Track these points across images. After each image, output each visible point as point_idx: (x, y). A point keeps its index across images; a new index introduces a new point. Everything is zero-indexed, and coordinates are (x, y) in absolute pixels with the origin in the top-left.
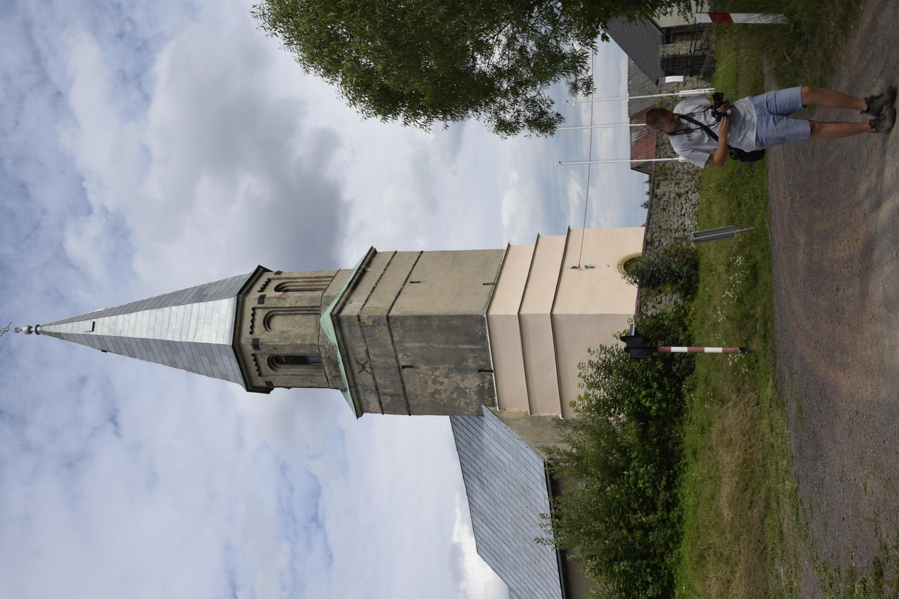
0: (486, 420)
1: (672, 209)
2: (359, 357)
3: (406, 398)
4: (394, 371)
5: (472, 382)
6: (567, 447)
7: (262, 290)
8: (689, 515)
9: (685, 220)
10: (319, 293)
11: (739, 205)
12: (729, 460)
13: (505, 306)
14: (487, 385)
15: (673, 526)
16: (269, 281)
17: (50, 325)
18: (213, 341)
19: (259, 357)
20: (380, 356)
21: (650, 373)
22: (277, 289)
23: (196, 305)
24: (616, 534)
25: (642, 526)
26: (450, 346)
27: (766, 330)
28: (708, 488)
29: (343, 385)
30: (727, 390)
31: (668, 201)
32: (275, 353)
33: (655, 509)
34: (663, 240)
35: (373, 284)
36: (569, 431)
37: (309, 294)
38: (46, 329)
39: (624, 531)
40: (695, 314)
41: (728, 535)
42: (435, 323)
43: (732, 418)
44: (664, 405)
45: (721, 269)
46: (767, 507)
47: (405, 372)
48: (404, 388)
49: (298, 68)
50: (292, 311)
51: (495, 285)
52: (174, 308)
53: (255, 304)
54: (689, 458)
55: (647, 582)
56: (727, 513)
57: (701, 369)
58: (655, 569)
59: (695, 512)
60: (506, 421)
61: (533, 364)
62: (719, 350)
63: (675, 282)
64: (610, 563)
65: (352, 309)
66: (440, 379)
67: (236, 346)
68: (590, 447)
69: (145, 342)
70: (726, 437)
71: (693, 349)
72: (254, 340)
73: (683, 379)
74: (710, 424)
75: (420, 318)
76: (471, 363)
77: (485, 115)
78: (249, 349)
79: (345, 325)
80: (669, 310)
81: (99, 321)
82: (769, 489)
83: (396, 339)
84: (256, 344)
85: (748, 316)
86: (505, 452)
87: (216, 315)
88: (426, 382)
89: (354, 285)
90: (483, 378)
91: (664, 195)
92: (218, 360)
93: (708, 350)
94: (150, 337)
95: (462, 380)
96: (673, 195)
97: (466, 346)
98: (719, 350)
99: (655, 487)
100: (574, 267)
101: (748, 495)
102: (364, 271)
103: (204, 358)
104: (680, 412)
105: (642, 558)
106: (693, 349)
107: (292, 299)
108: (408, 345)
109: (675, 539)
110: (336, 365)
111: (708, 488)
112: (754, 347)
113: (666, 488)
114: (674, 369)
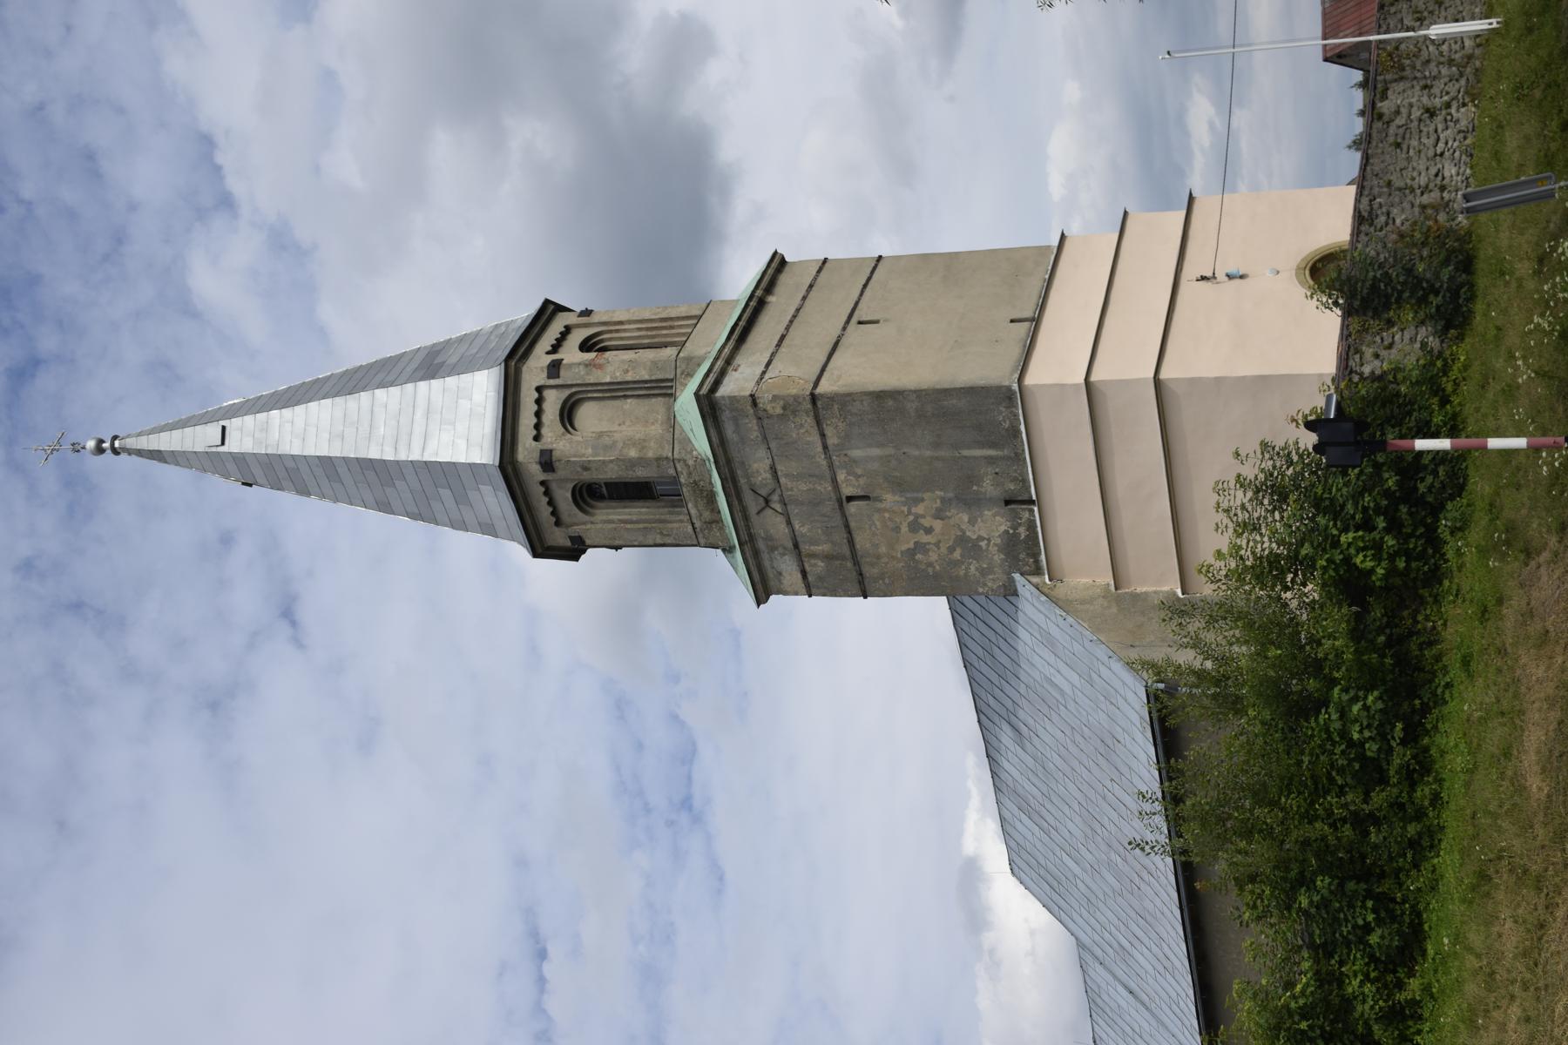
1: (1414, 143)
3: (856, 563)
4: (829, 506)
5: (993, 526)
7: (555, 348)
8: (1454, 789)
9: (1443, 166)
10: (670, 352)
13: (1057, 364)
14: (1023, 532)
15: (1420, 815)
19: (554, 486)
21: (1371, 501)
22: (586, 346)
23: (422, 385)
28: (1495, 735)
29: (728, 539)
31: (1406, 127)
32: (587, 477)
33: (1383, 781)
34: (1395, 211)
35: (781, 329)
36: (1195, 625)
37: (649, 354)
38: (131, 443)
40: (1466, 367)
41: (1540, 831)
42: (911, 406)
45: (1524, 268)
47: (852, 508)
50: (617, 391)
51: (1036, 321)
52: (380, 393)
53: (541, 378)
54: (1455, 672)
56: (1537, 785)
57: (1479, 486)
58: (1384, 903)
59: (1467, 785)
60: (1065, 605)
62: (1520, 443)
65: (738, 383)
66: (926, 522)
69: (327, 464)
70: (1535, 628)
71: (1462, 442)
72: (542, 452)
73: (1442, 507)
74: (1500, 602)
75: (879, 396)
76: (988, 487)
78: (534, 472)
79: (726, 416)
80: (1410, 362)
81: (233, 424)
83: (832, 440)
84: (547, 462)
87: (464, 404)
88: (897, 529)
89: (742, 332)
91: (1398, 112)
93: (1494, 443)
94: (336, 451)
95: (972, 522)
96: (1416, 113)
98: (1520, 443)
100: (1203, 278)
103: (445, 493)
104: (1435, 576)
106: (1462, 442)
107: (615, 366)
108: (856, 453)
109: (1423, 846)
110: (711, 498)
111: (1495, 735)
113: (1403, 742)
114: (1422, 488)
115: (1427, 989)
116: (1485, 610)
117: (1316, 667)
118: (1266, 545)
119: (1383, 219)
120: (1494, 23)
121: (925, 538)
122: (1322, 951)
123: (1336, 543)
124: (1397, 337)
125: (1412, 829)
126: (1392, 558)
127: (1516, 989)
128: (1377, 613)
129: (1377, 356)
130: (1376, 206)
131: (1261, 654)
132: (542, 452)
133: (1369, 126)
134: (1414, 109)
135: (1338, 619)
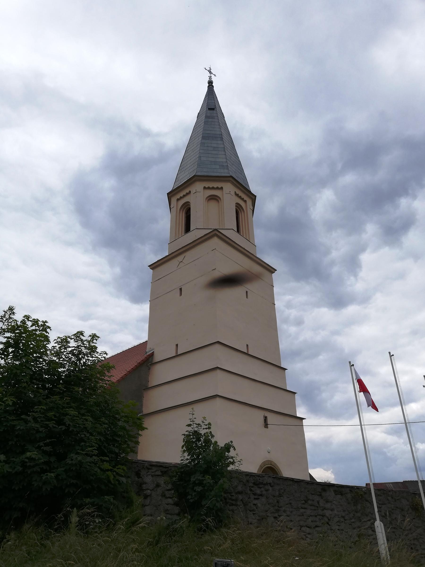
16: (245, 201)
34: (263, 499)
68: (371, 229)
91: (327, 502)
119: (258, 492)
124: (170, 501)
129: (158, 486)
130: (267, 487)
133: (320, 484)
134: (330, 512)
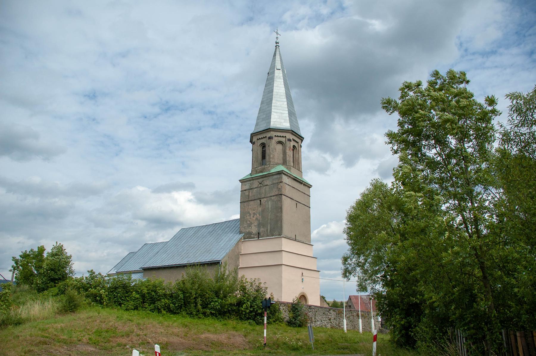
0: (238, 235)
2: (265, 181)
3: (247, 201)
4: (259, 196)
5: (254, 230)
6: (227, 273)
7: (294, 140)
8: (200, 321)
9: (319, 322)
10: (292, 164)
11: (323, 344)
12: (223, 337)
13: (286, 245)
14: (253, 236)
15: (196, 315)
17: (280, 54)
18: (272, 120)
19: (265, 139)
20: (265, 191)
21: (256, 309)
22: (294, 146)
23: (287, 112)
24: (193, 292)
25: (196, 303)
26: (269, 221)
27: (273, 353)
28: (211, 329)
29: (253, 174)
30: (250, 338)
32: (267, 146)
33: (203, 308)
35: (296, 187)
36: (233, 274)
37: (292, 160)
38: (278, 49)
39: (194, 296)
40: (280, 325)
41: (195, 336)
42: (279, 214)
43: (239, 340)
44: (244, 313)
45: (298, 336)
46: (206, 351)
47: (259, 201)
48: (252, 200)
49: (362, 191)
50: (284, 153)
51: (295, 240)
52: (286, 103)
53: (287, 137)
54: (223, 322)
55: (175, 304)
56: (203, 336)
57: (258, 328)
58: (180, 307)
59: (202, 324)
60: (237, 244)
61: (261, 256)
62: (265, 335)
63: (294, 318)
64: (181, 290)
65: (285, 179)
66: (255, 216)
67: (269, 130)
69: (272, 91)
70: (231, 337)
71: (266, 325)
72: (272, 137)
73: (254, 321)
74: (236, 331)
75: (281, 208)
76: (262, 229)
77: (349, 253)
78: (268, 135)
79: (278, 176)
80: (282, 315)
81: (281, 72)
82: (212, 352)
83: (272, 198)
84: (270, 138)
85: (278, 346)
86: (224, 243)
87: (283, 121)
88: (254, 210)
89: (295, 179)
90: (256, 235)
92: (264, 122)
93: (265, 331)
94: (274, 93)
95: (255, 226)
96: (330, 317)
97: (269, 227)
98: (265, 335)
99: (211, 309)
101: (210, 344)
102: (302, 183)
103: (265, 116)
104: (241, 319)
105: (184, 303)
106: (266, 325)
107: (290, 153)
108: (270, 203)
109: (191, 314)
110: (261, 172)
111: (211, 329)
112: (266, 348)
113: (211, 313)
114: (258, 317)
115: (164, 314)
116: (235, 328)
117: (225, 297)
118: (248, 287)
120: (346, 331)
121: (252, 216)
122: (171, 296)
123: (248, 301)
125: (194, 313)
126: (245, 311)
127: (167, 331)
128: (235, 308)
131: (228, 287)
132: (272, 137)
135: (234, 301)
